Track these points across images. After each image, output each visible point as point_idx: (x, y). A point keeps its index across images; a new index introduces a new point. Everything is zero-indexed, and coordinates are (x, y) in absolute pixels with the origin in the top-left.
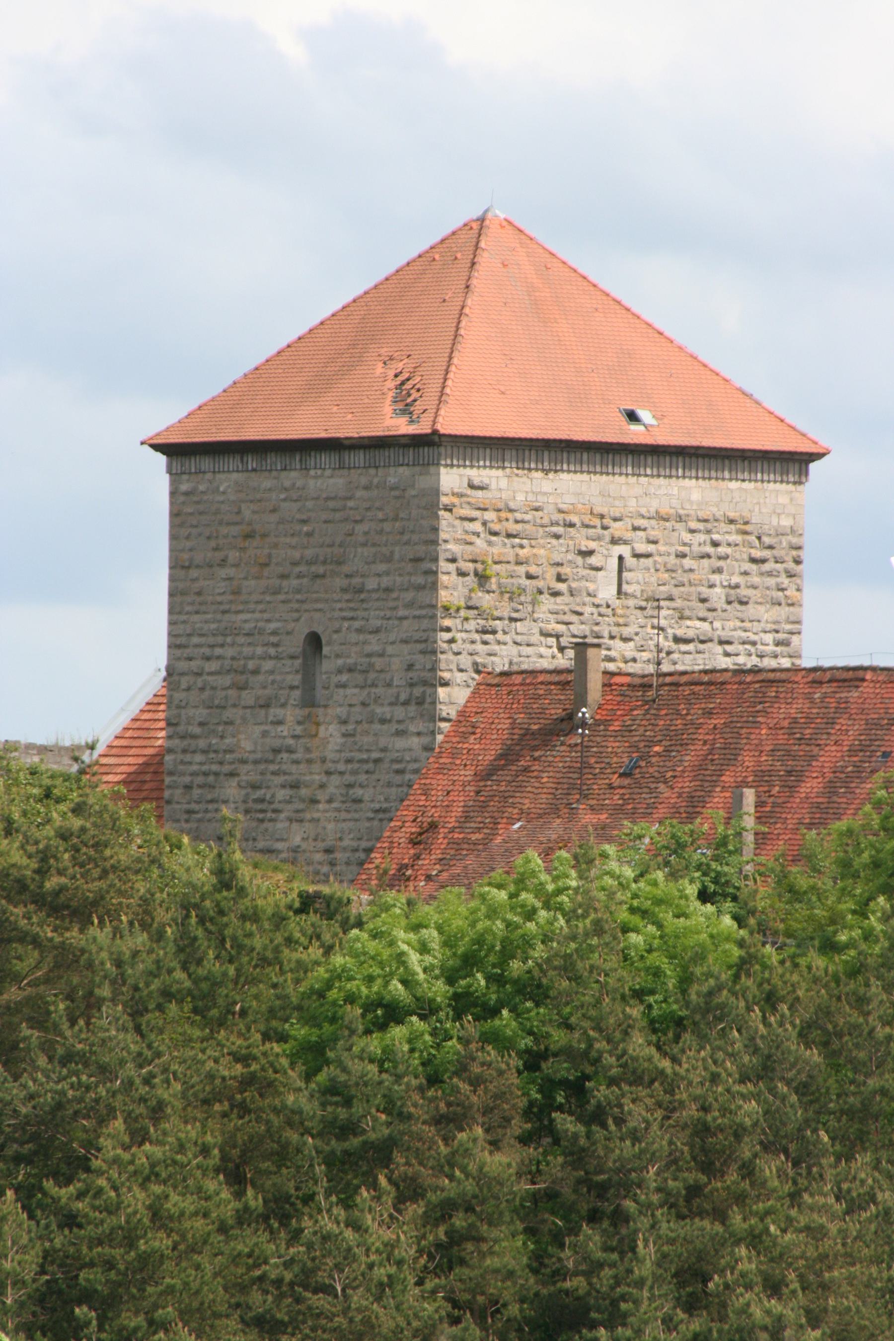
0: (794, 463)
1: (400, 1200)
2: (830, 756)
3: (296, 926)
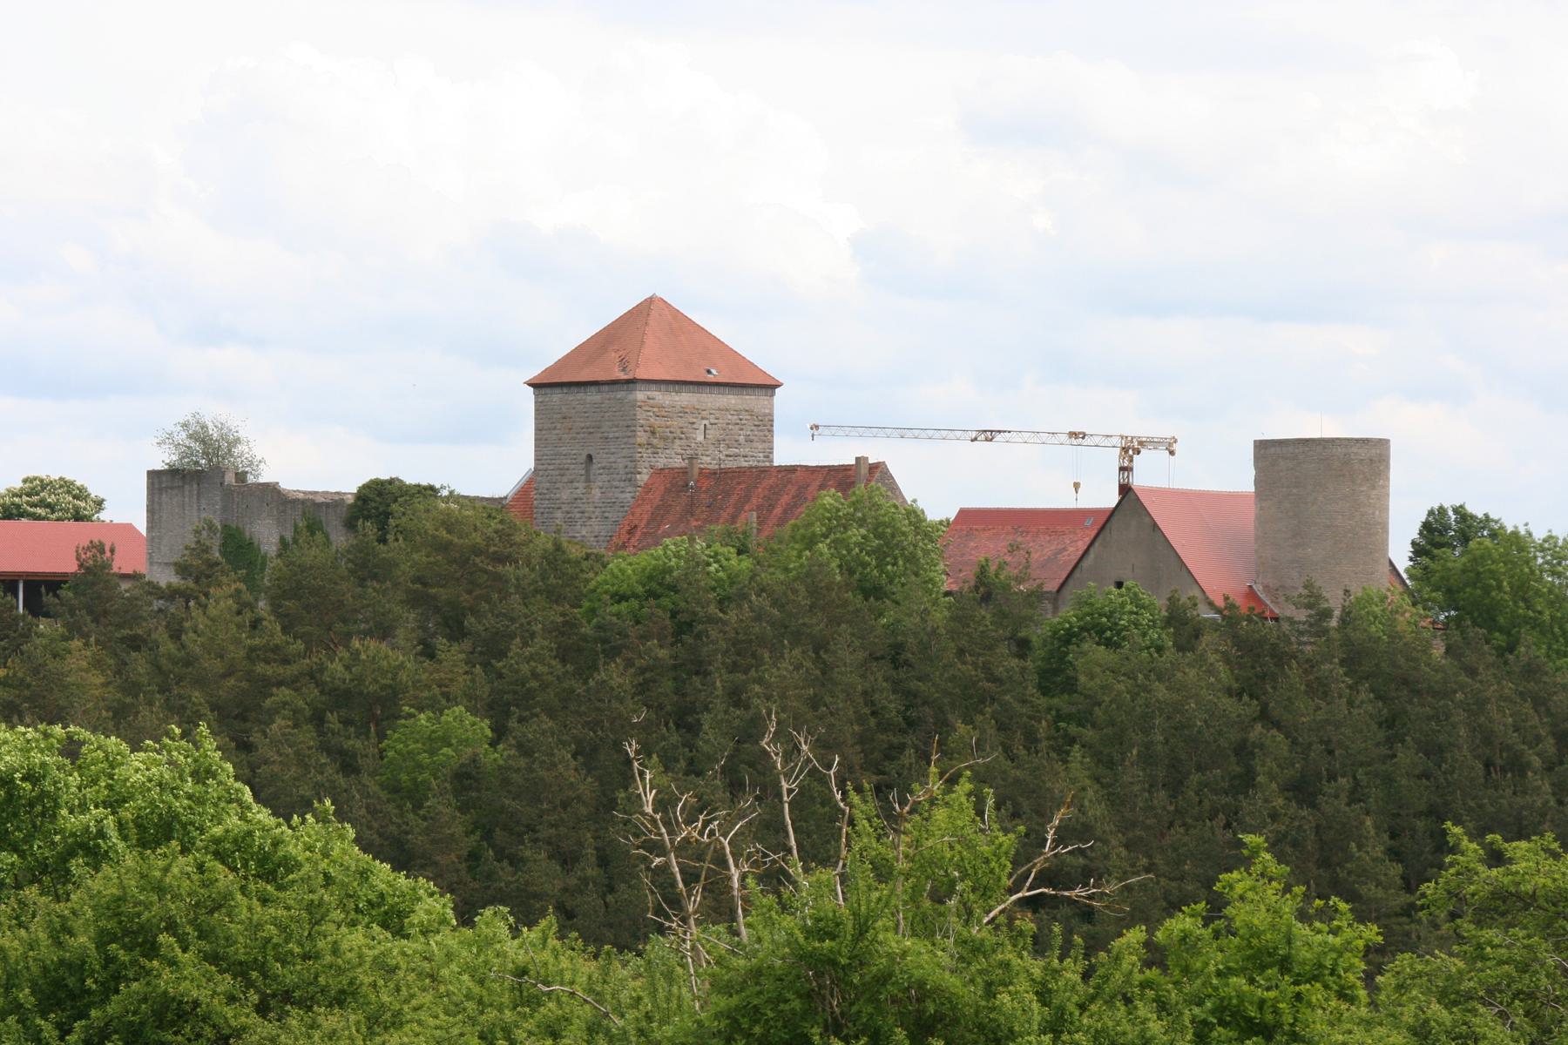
0: (770, 387)
1: (625, 668)
2: (785, 499)
3: (585, 565)
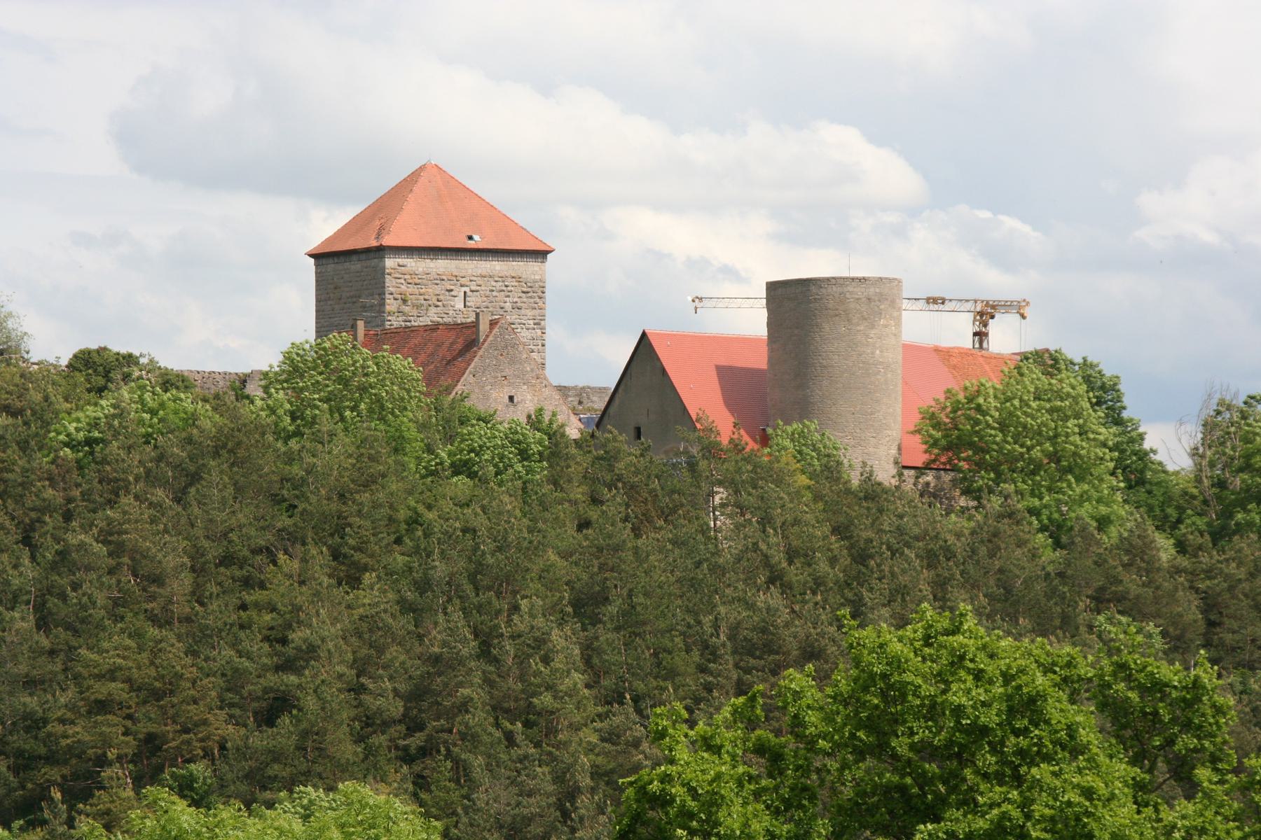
0: (541, 254)
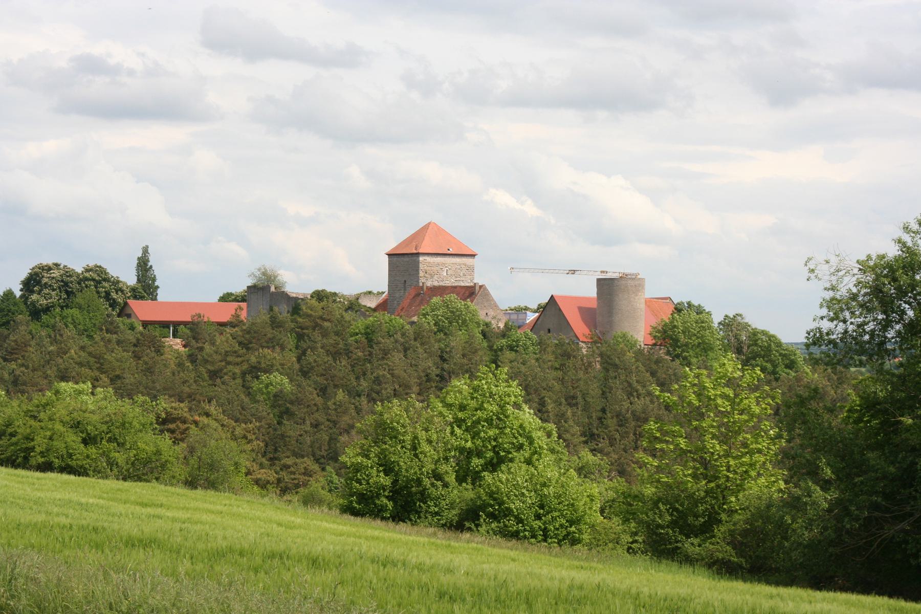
0: (473, 256)
